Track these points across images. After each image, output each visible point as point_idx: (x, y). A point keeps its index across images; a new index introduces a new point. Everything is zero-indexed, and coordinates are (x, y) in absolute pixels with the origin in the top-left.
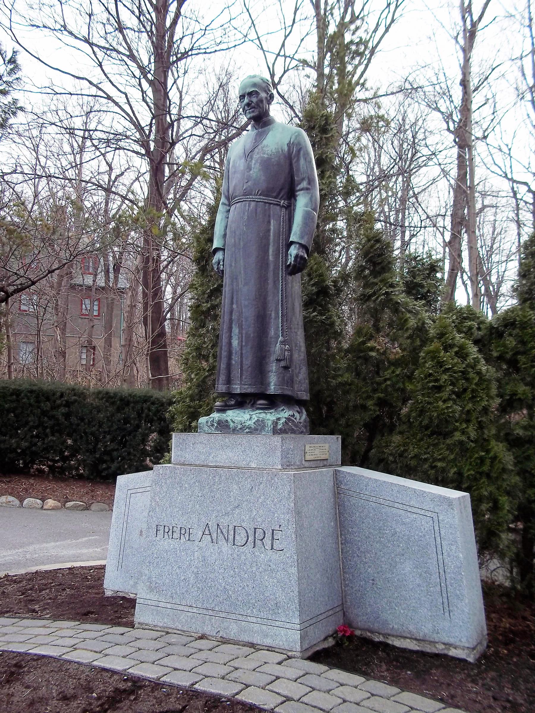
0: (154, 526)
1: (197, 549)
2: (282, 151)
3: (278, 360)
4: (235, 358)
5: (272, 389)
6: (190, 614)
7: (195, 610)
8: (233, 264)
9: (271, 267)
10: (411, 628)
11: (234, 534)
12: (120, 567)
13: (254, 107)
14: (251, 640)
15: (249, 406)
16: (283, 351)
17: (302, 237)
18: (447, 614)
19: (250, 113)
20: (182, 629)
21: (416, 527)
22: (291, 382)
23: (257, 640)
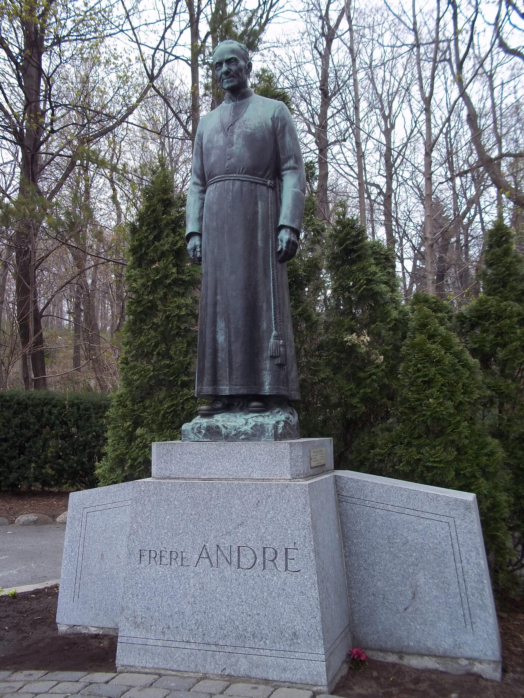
0: (137, 551)
1: (192, 575)
2: (266, 125)
3: (273, 357)
4: (222, 356)
5: (267, 389)
6: (186, 651)
7: (193, 646)
8: (216, 251)
9: (261, 254)
10: (429, 644)
11: (239, 556)
12: (76, 597)
13: (233, 76)
14: (265, 676)
15: (238, 408)
16: (278, 346)
17: (293, 221)
18: (469, 627)
19: (228, 82)
20: (178, 669)
21: (431, 534)
22: (286, 381)
23: (273, 675)
